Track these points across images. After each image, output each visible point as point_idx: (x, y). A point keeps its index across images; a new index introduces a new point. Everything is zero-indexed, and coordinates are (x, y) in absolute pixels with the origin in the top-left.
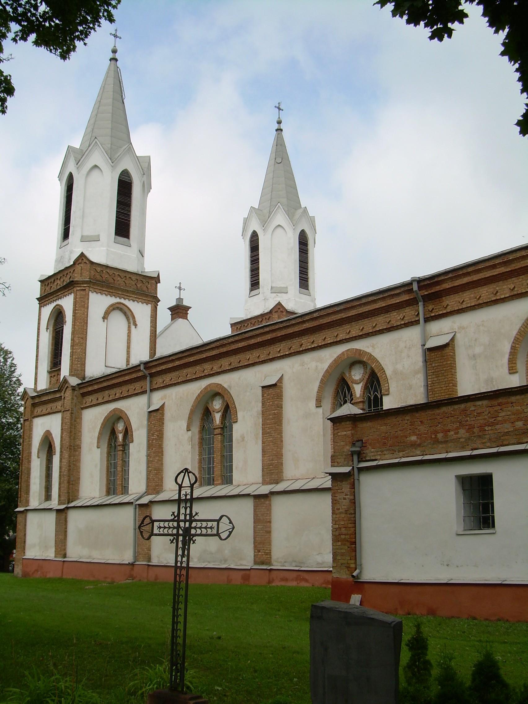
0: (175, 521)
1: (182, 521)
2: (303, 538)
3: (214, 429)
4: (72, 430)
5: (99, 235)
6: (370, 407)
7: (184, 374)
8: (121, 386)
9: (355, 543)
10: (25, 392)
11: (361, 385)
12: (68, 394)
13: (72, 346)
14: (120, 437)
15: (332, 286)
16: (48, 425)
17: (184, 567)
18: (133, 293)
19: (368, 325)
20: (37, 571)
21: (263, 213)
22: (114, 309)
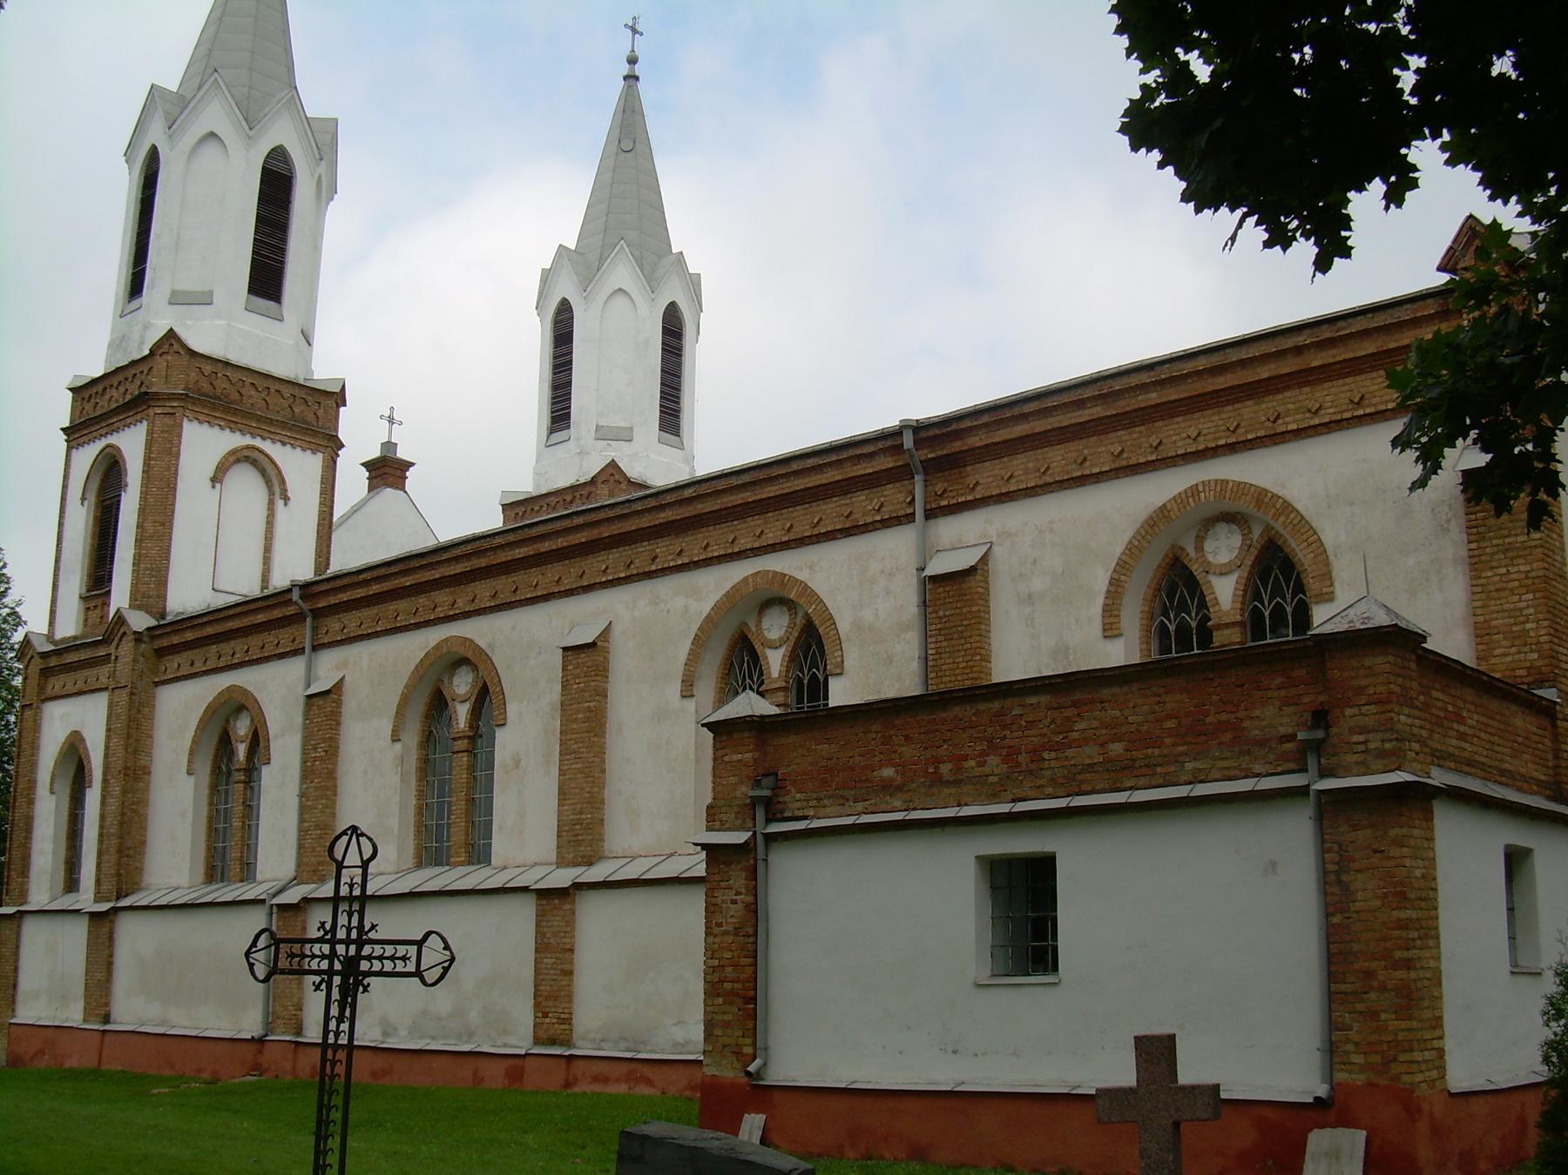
0: (327, 942)
1: (341, 942)
2: (642, 987)
3: (454, 739)
4: (132, 732)
5: (211, 292)
6: (800, 700)
7: (337, 626)
8: (247, 636)
9: (754, 1000)
10: (27, 642)
11: (782, 651)
12: (126, 649)
13: (139, 541)
14: (241, 750)
15: (734, 427)
16: (78, 718)
17: (342, 1046)
18: (283, 425)
19: (801, 519)
20: (41, 1052)
21: (581, 262)
22: (238, 461)
